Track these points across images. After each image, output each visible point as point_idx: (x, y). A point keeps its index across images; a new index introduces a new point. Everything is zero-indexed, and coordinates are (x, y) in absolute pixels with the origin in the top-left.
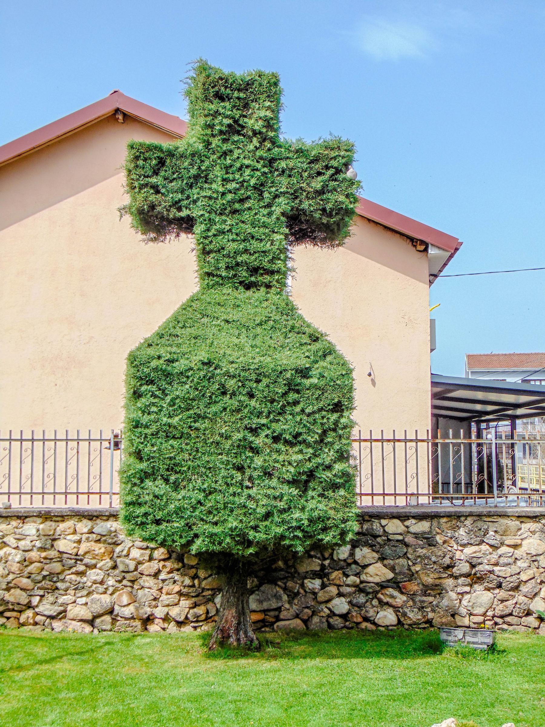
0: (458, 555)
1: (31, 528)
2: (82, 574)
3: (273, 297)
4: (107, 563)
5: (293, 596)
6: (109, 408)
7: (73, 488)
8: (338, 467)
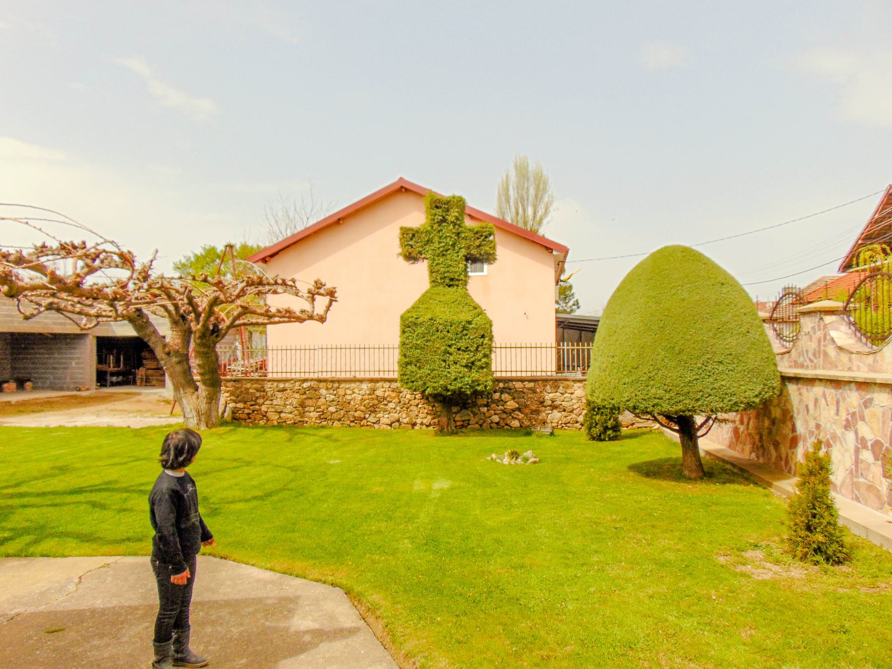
0: (546, 397)
1: (365, 386)
2: (386, 405)
3: (460, 289)
4: (396, 400)
5: (475, 414)
6: (394, 337)
7: (382, 369)
8: (483, 360)
